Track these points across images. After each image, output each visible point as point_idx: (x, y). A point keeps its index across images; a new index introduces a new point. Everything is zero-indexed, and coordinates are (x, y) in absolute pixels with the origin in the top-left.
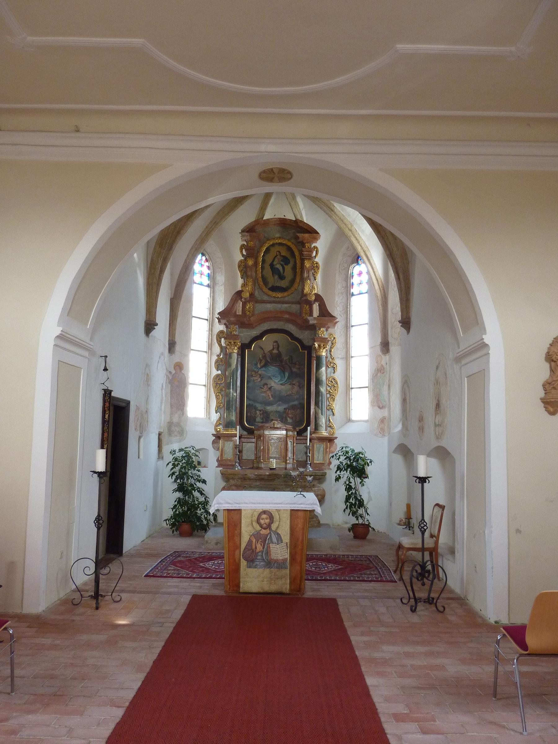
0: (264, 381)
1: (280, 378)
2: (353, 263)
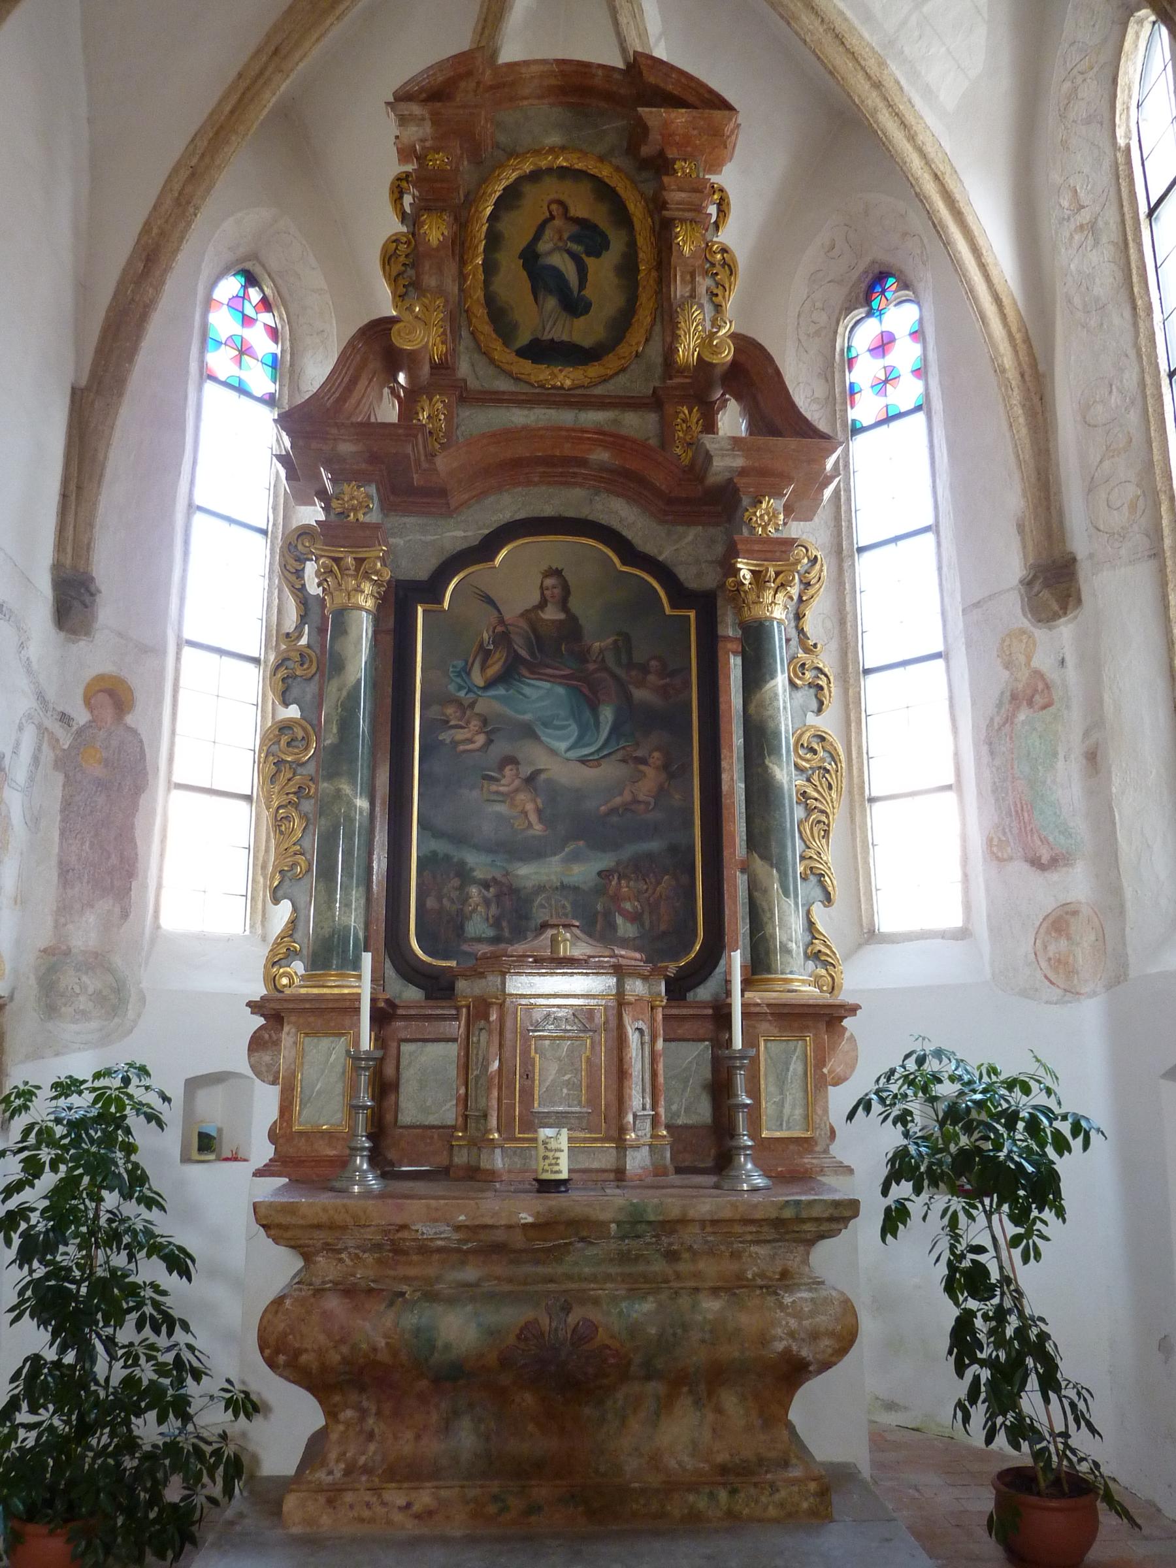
0: (501, 748)
1: (574, 730)
2: (849, 310)
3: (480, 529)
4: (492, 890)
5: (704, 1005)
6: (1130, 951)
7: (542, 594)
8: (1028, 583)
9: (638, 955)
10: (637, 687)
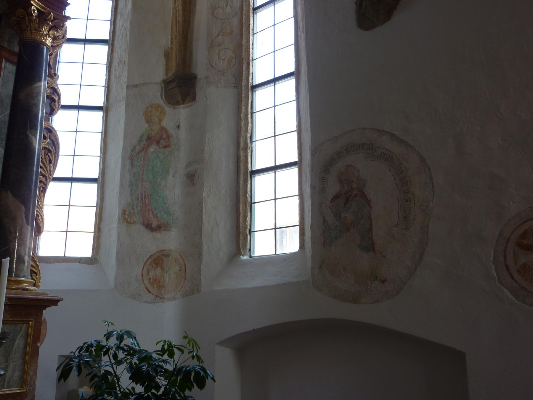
6: (202, 278)
8: (166, 83)
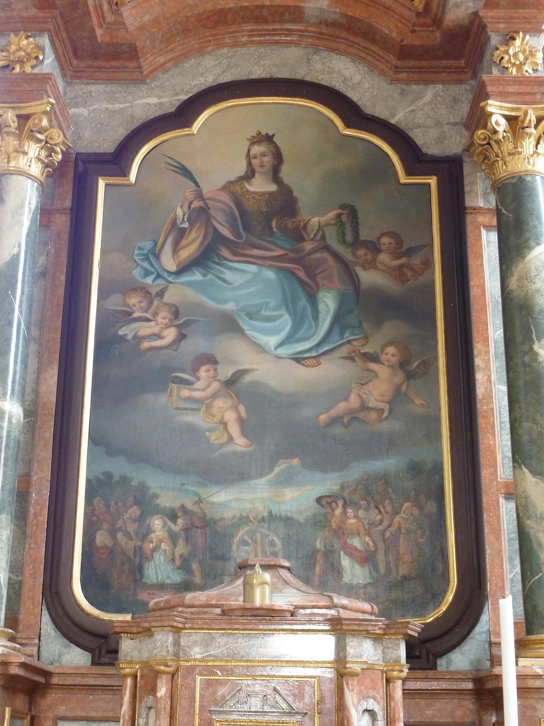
0: (196, 344)
1: (286, 322)
3: (177, 94)
4: (180, 521)
5: (455, 676)
7: (249, 164)
9: (367, 606)
10: (365, 269)
